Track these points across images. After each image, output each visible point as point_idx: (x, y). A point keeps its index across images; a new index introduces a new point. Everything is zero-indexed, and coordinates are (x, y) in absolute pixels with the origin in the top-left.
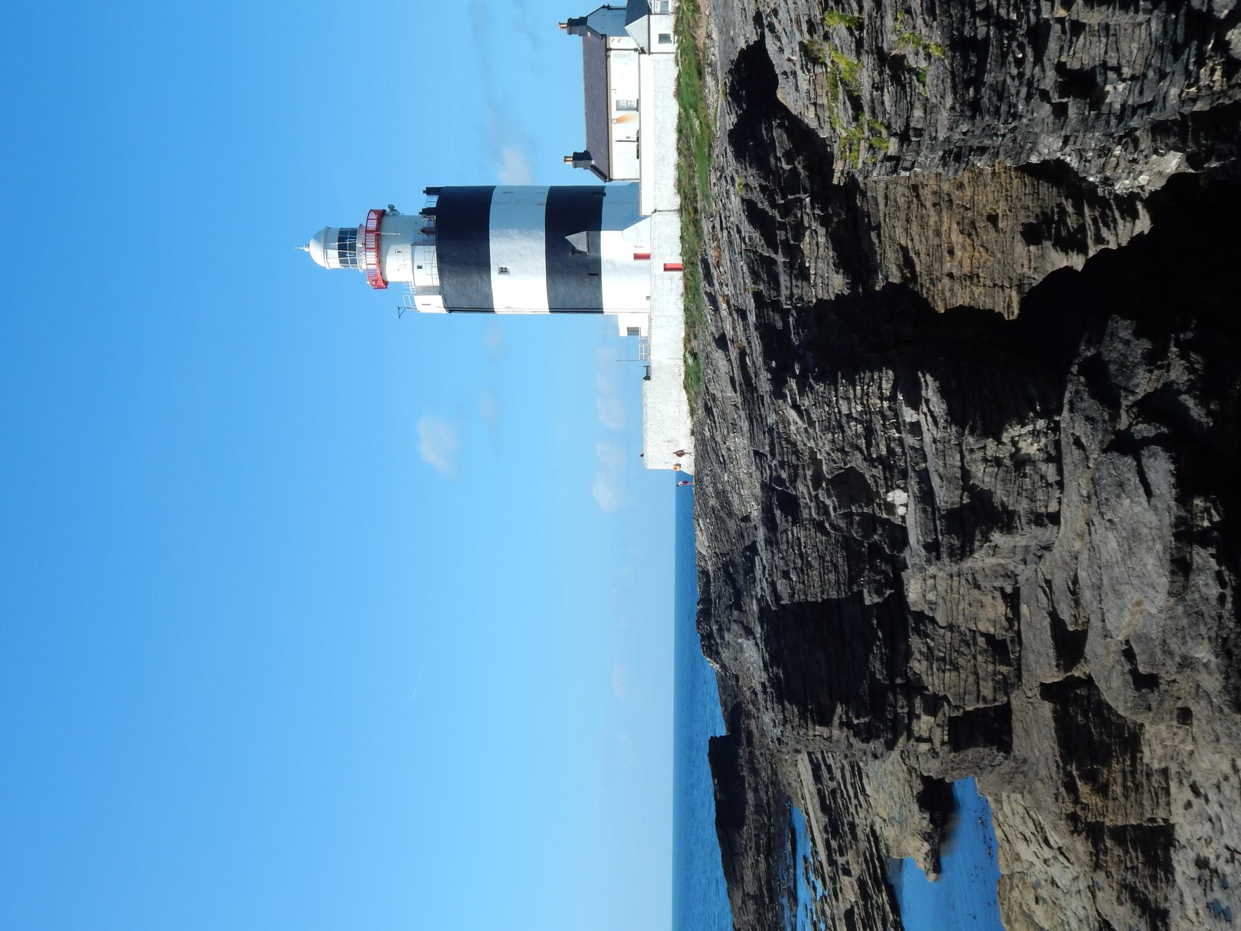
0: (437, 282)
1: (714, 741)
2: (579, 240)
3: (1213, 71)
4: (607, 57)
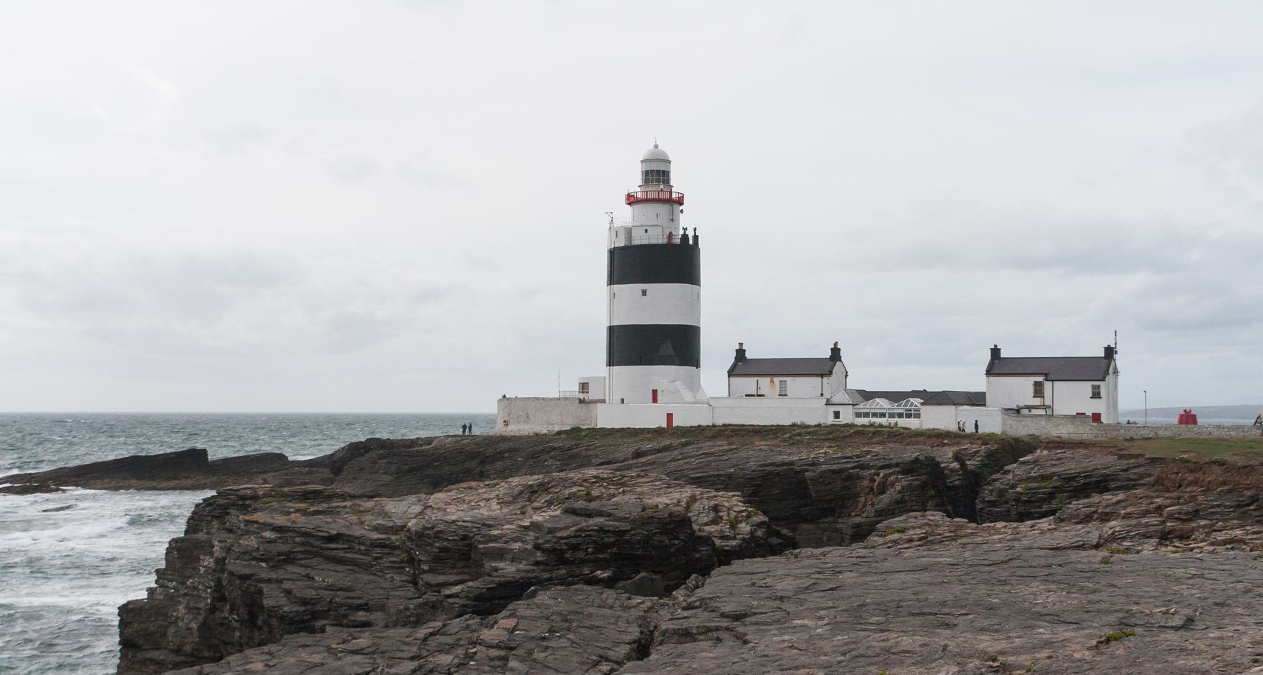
4: (817, 375)
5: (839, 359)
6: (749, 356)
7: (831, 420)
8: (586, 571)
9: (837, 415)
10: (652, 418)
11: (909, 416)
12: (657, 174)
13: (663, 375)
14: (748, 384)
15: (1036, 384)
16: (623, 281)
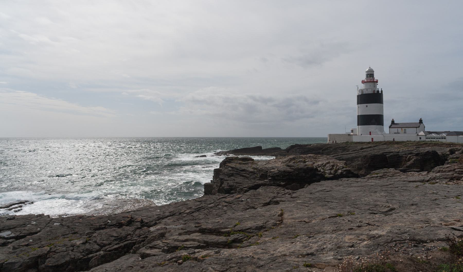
6: (395, 122)
7: (419, 140)
8: (278, 182)
9: (420, 138)
10: (367, 139)
11: (442, 139)
12: (370, 74)
13: (372, 128)
14: (395, 130)
16: (361, 103)
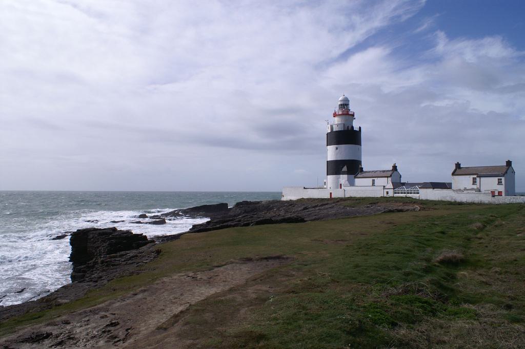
0: (334, 130)
1: (227, 204)
2: (345, 169)
3: (157, 284)
4: (385, 177)
5: (396, 170)
9: (387, 193)
15: (474, 178)
